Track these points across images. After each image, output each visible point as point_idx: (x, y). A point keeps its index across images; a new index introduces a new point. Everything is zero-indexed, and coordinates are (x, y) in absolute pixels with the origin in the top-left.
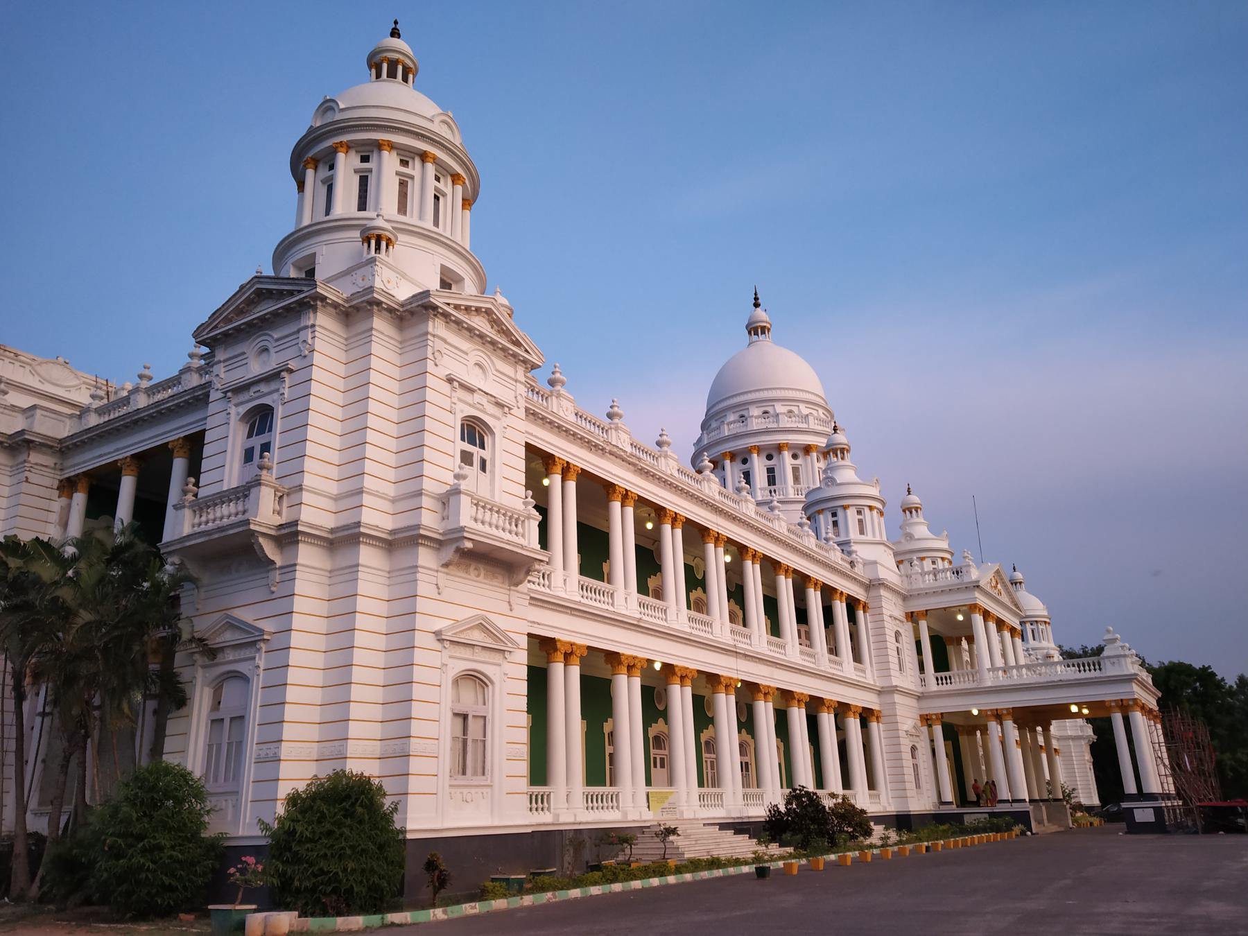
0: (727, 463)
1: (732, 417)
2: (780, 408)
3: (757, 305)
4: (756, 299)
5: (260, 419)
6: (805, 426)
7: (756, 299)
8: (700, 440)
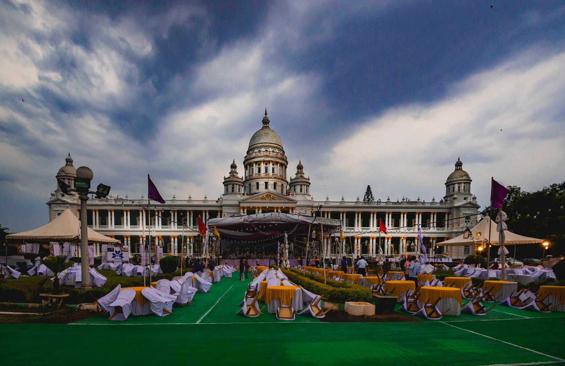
0: (254, 165)
1: (256, 150)
2: (263, 149)
8: (246, 157)
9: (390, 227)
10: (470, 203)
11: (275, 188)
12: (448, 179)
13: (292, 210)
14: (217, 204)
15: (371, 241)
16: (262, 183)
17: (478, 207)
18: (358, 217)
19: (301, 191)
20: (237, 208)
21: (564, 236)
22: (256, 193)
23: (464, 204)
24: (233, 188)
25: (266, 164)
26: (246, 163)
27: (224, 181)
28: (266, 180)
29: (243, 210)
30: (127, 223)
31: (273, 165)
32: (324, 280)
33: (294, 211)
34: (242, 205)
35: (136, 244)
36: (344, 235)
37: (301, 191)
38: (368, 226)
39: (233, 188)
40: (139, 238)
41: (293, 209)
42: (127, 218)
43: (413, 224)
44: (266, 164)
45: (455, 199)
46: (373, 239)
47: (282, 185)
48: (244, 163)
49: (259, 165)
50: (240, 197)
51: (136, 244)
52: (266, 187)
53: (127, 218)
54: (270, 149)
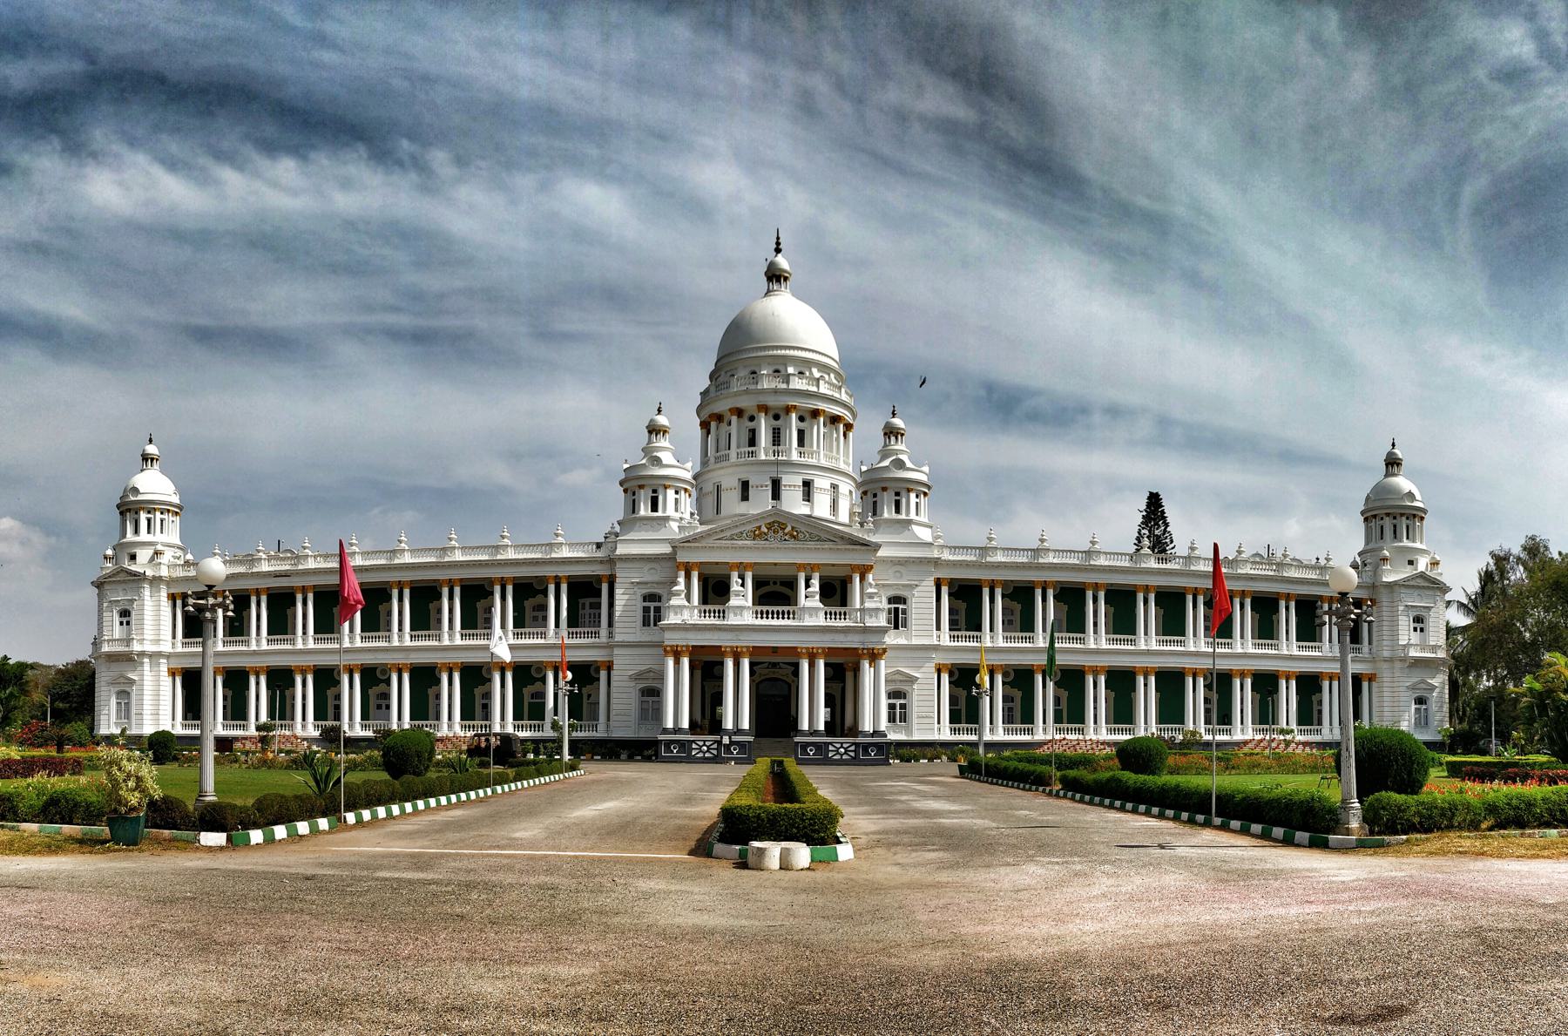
3: (778, 250)
4: (778, 244)
5: (125, 613)
6: (814, 389)
7: (778, 244)
9: (815, 602)
10: (1422, 576)
12: (1368, 498)
14: (599, 554)
17: (1444, 589)
20: (669, 564)
23: (1405, 580)
25: (776, 417)
26: (706, 413)
27: (623, 476)
31: (801, 419)
33: (870, 577)
34: (682, 557)
35: (478, 691)
38: (1183, 634)
40: (489, 671)
41: (864, 571)
42: (451, 609)
44: (776, 417)
45: (1385, 559)
47: (834, 487)
49: (752, 419)
51: (478, 691)
53: (451, 609)
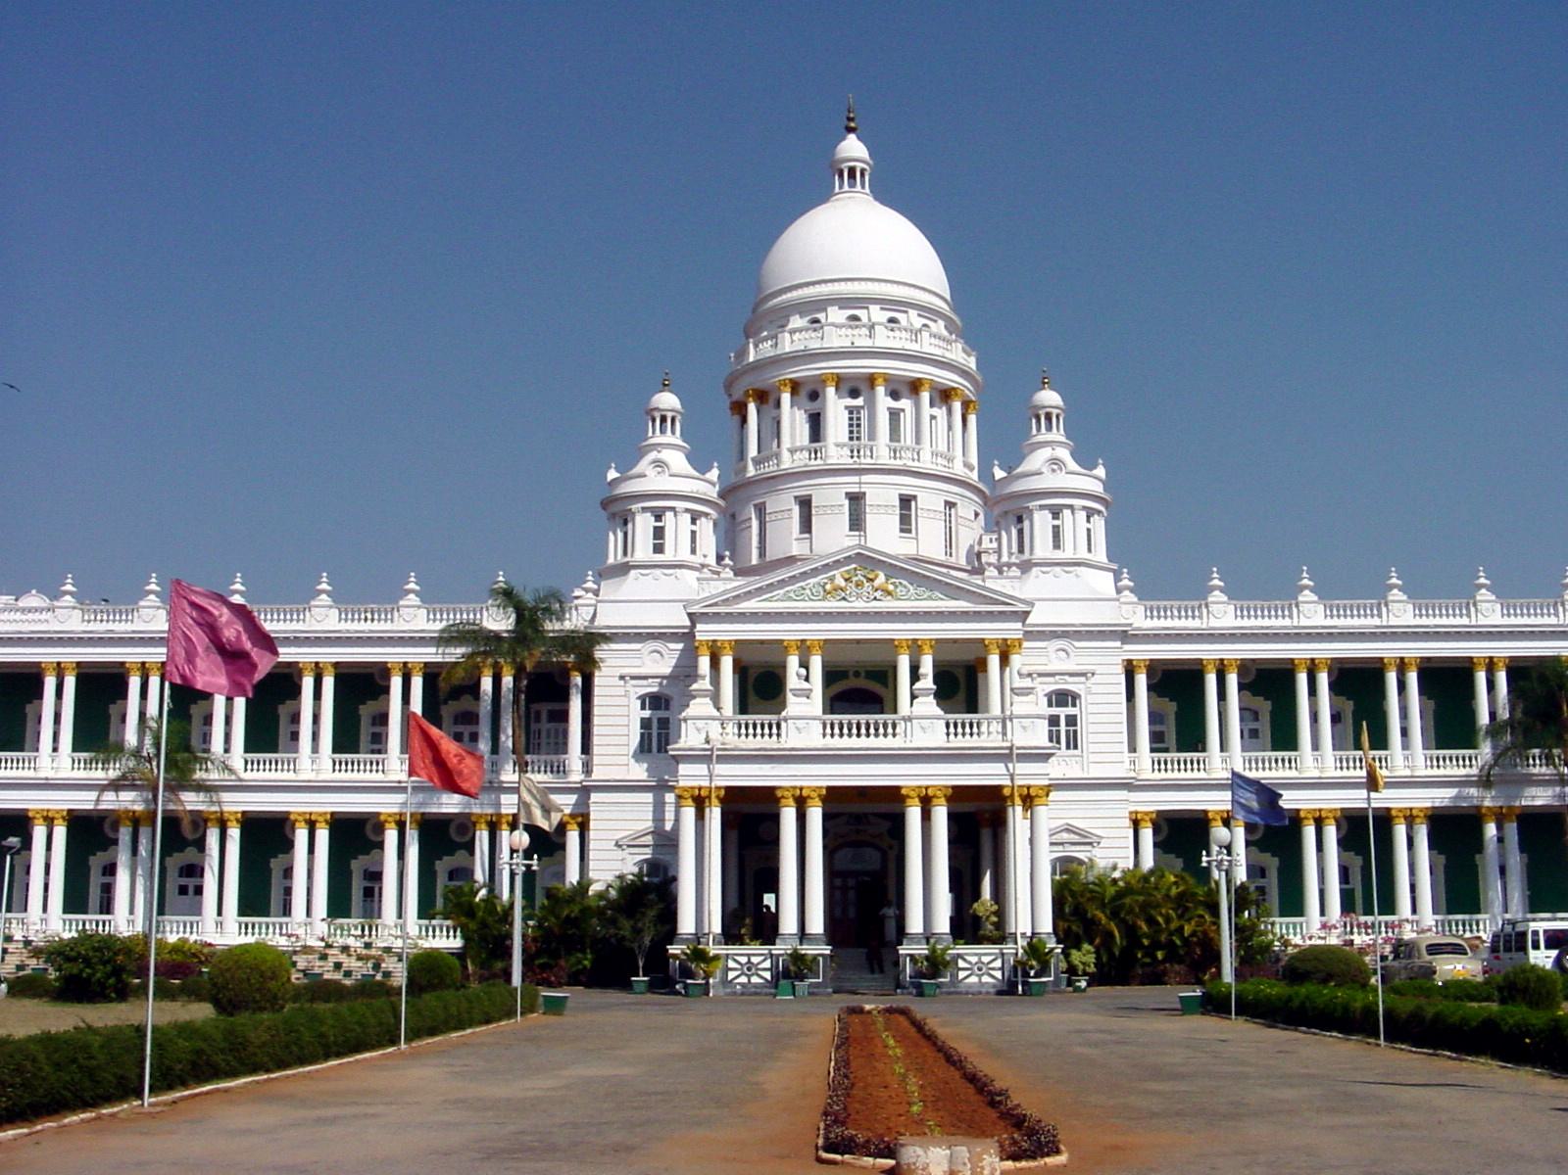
2: (837, 315)
9: (238, 756)
11: (905, 523)
13: (1005, 660)
15: (39, 833)
16: (830, 497)
18: (1402, 686)
19: (659, 549)
21: (1566, 771)
22: (791, 560)
24: (659, 533)
28: (908, 485)
29: (804, 664)
30: (315, 736)
32: (1370, 1012)
33: (1016, 660)
34: (705, 632)
36: (236, 803)
37: (659, 549)
39: (659, 533)
40: (380, 828)
43: (284, 730)
46: (49, 821)
48: (729, 386)
50: (688, 585)
52: (857, 523)
54: (878, 314)
